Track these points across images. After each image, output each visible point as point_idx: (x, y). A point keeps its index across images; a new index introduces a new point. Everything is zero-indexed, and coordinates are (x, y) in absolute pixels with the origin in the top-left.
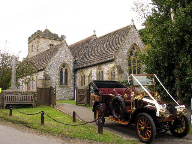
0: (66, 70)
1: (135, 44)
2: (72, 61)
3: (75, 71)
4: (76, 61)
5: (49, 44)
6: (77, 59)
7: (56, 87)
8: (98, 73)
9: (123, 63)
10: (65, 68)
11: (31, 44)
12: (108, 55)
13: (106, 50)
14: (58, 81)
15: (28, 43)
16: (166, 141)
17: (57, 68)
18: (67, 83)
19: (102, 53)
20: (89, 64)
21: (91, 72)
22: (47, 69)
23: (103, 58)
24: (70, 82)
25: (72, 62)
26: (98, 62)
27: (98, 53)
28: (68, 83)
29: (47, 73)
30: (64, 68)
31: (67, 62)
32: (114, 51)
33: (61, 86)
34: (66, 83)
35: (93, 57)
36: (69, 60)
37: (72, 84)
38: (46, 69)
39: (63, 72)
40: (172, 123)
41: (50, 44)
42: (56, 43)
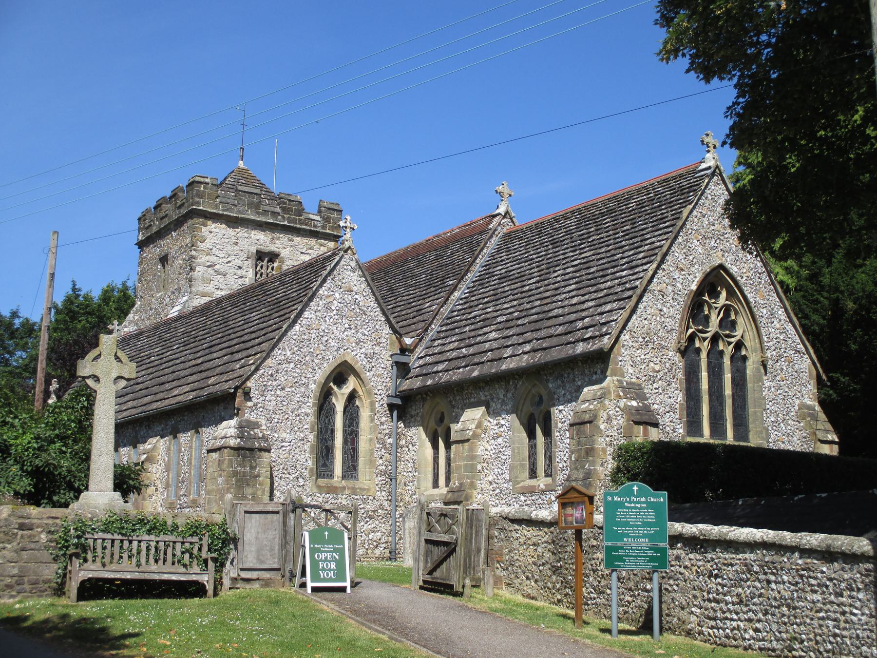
0: (352, 397)
2: (386, 354)
4: (404, 350)
5: (253, 249)
6: (408, 341)
7: (586, 623)
9: (657, 368)
10: (347, 389)
11: (154, 252)
12: (580, 324)
13: (569, 296)
14: (307, 459)
15: (141, 245)
16: (50, 314)
17: (306, 385)
18: (355, 468)
19: (545, 317)
20: (476, 373)
23: (554, 341)
24: (371, 463)
27: (525, 313)
31: (356, 357)
32: (608, 307)
33: (322, 482)
34: (351, 469)
35: (493, 335)
36: (368, 348)
37: (383, 473)
39: (332, 410)
40: (854, 386)
41: (258, 252)
42: (294, 252)
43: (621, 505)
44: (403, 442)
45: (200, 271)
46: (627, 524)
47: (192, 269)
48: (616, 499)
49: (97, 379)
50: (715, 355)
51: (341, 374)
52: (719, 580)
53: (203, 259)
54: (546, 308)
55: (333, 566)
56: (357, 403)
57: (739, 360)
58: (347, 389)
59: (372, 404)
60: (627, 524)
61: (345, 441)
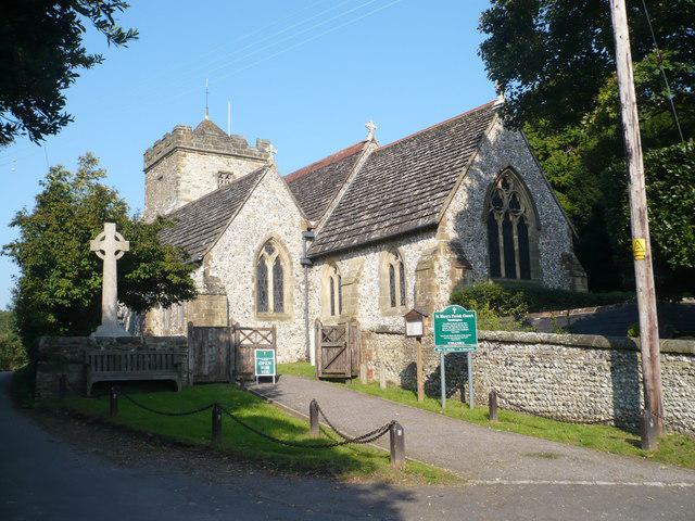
0: (278, 260)
1: (509, 167)
3: (312, 261)
8: (387, 270)
10: (274, 255)
12: (420, 207)
14: (250, 300)
21: (362, 267)
22: (215, 259)
24: (292, 301)
25: (298, 234)
26: (386, 232)
27: (385, 202)
28: (286, 304)
29: (215, 275)
30: (270, 254)
31: (280, 232)
38: (210, 258)
43: (445, 320)
44: (311, 287)
45: (182, 186)
46: (449, 333)
47: (178, 185)
48: (442, 316)
49: (103, 252)
50: (507, 225)
51: (268, 245)
52: (513, 367)
53: (184, 177)
54: (398, 198)
55: (268, 368)
56: (282, 264)
57: (523, 228)
58: (274, 255)
59: (291, 263)
60: (449, 333)
61: (275, 288)
